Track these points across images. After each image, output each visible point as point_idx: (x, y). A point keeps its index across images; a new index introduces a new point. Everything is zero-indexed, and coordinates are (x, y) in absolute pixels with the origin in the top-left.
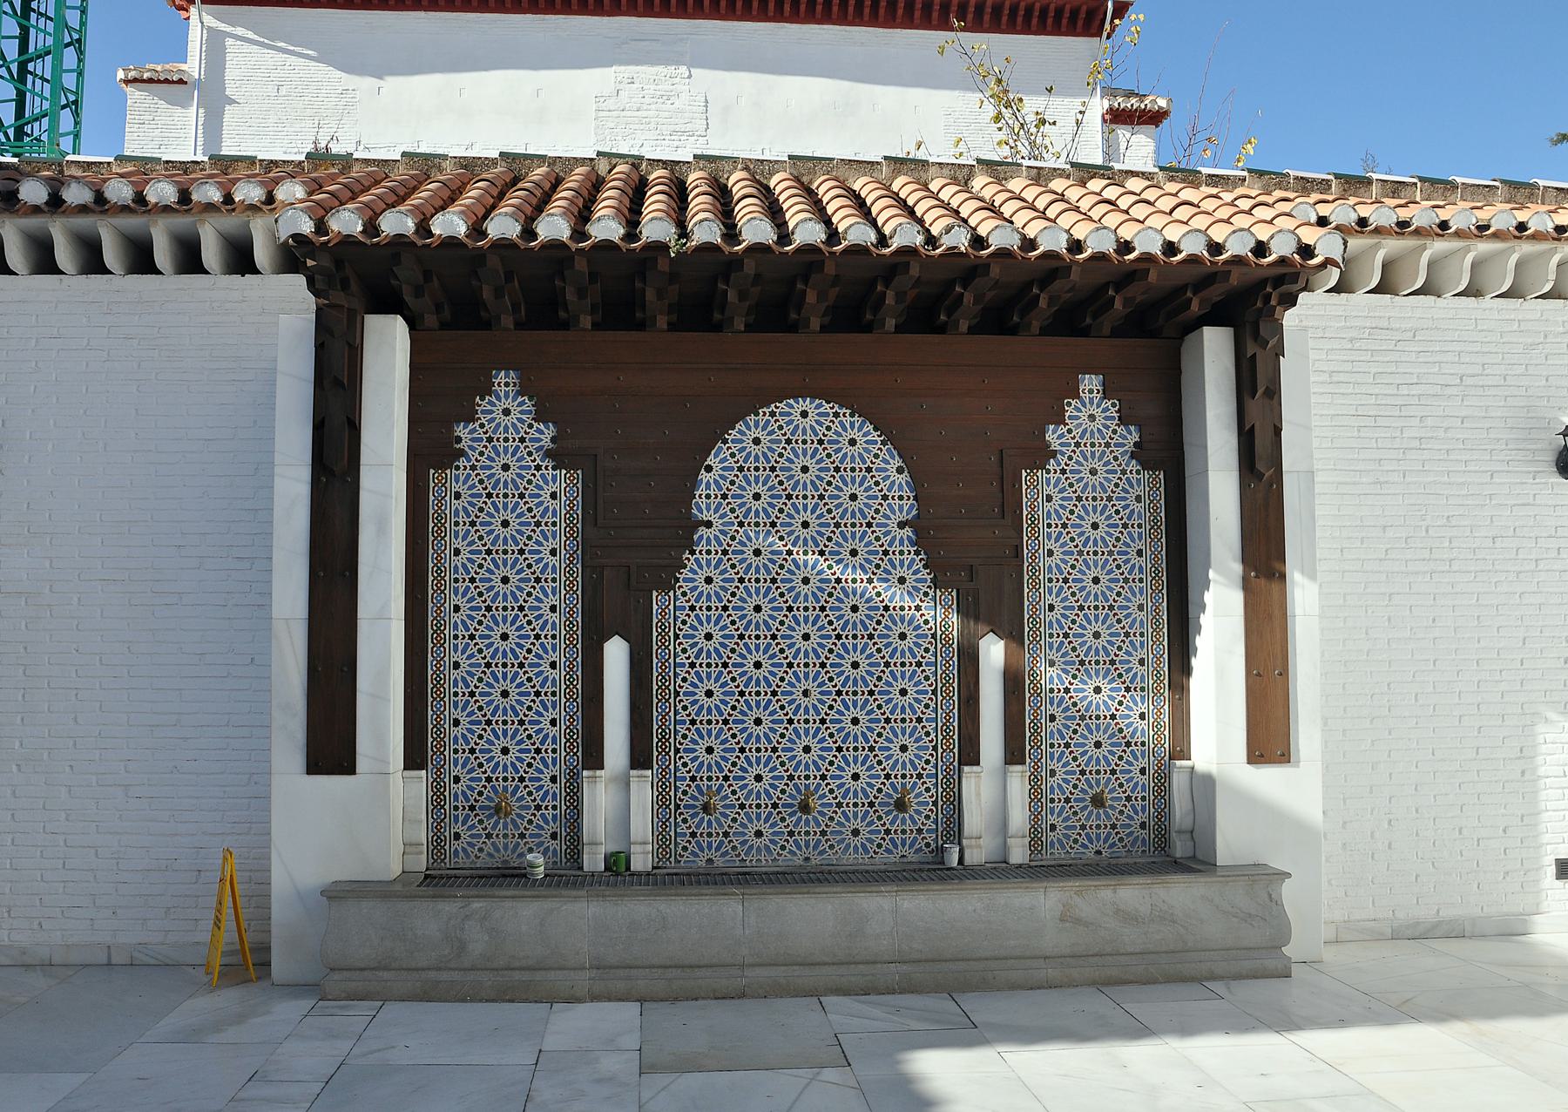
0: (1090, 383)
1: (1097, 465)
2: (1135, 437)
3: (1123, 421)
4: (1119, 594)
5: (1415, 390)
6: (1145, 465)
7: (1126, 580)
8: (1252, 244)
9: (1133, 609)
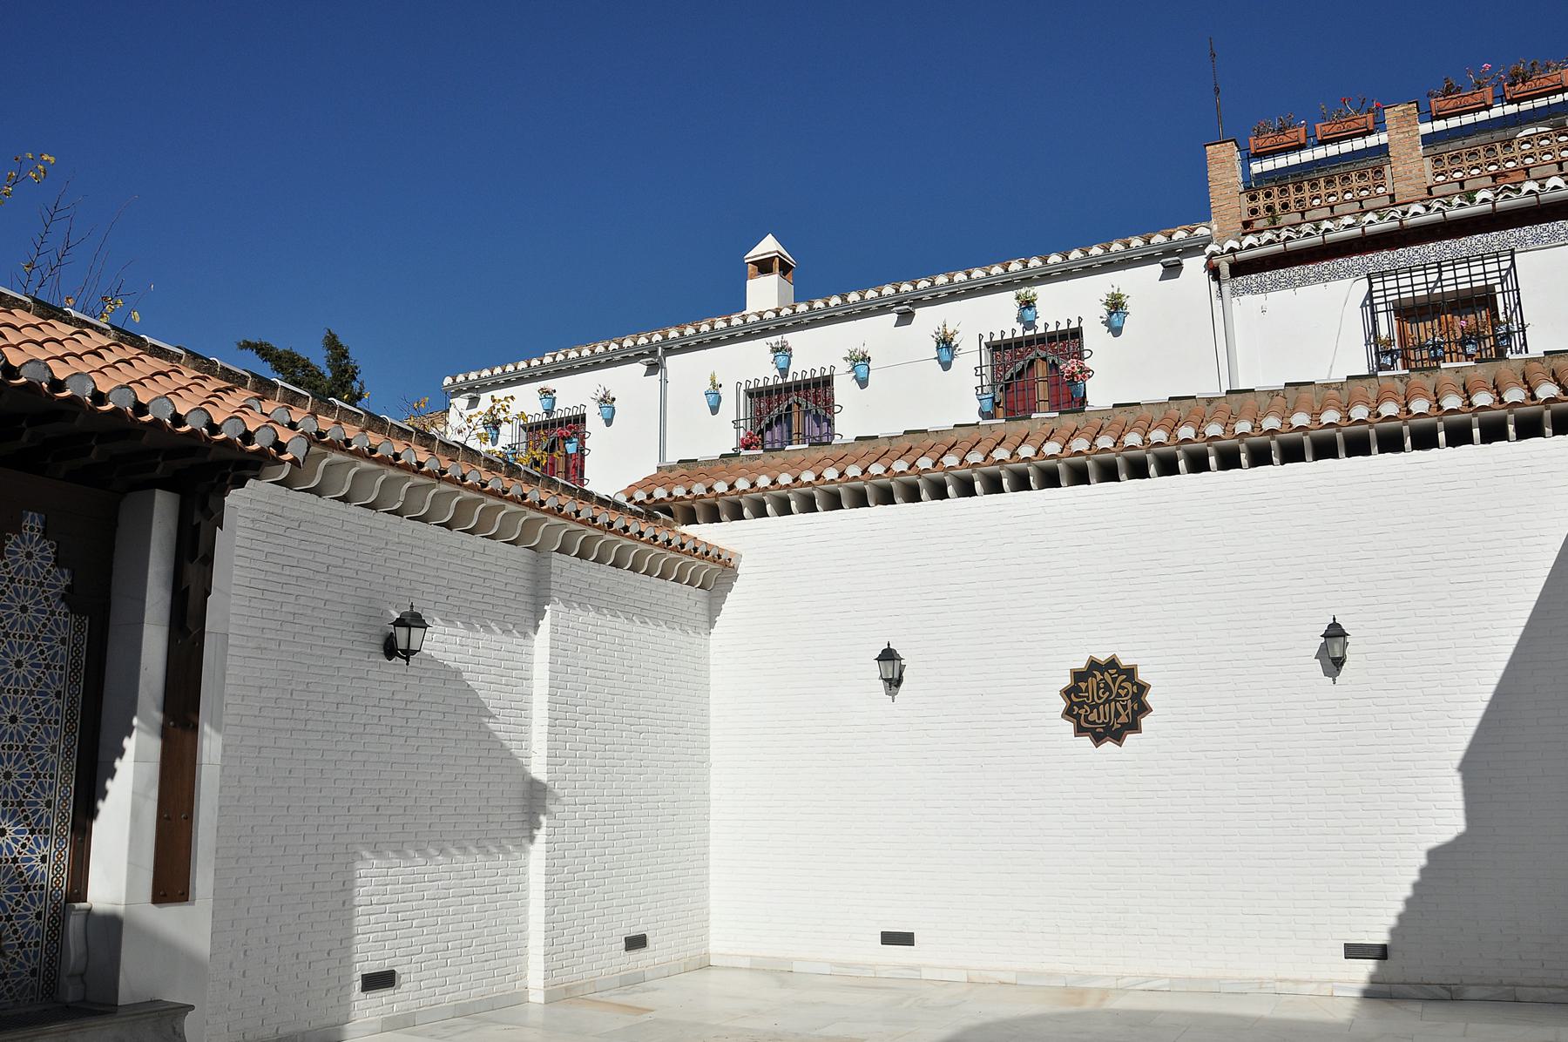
0: (32, 522)
1: (29, 603)
2: (66, 581)
3: (58, 563)
4: (34, 734)
5: (295, 572)
6: (74, 609)
7: (42, 721)
8: (242, 431)
9: (46, 751)
